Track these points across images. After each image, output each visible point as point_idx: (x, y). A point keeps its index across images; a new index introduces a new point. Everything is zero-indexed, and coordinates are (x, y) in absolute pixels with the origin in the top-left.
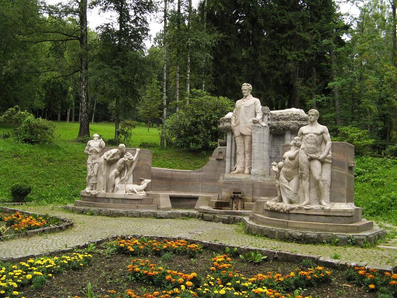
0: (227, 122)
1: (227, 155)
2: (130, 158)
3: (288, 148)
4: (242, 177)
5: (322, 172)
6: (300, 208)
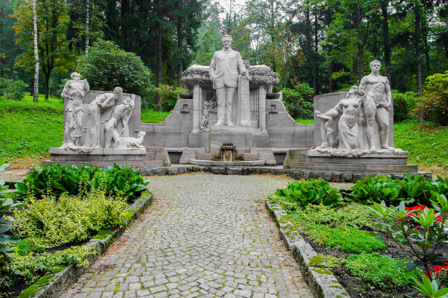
0: (196, 74)
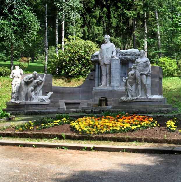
0: (96, 57)
1: (96, 77)
2: (41, 80)
3: (130, 70)
4: (106, 88)
5: (147, 80)
6: (137, 99)
